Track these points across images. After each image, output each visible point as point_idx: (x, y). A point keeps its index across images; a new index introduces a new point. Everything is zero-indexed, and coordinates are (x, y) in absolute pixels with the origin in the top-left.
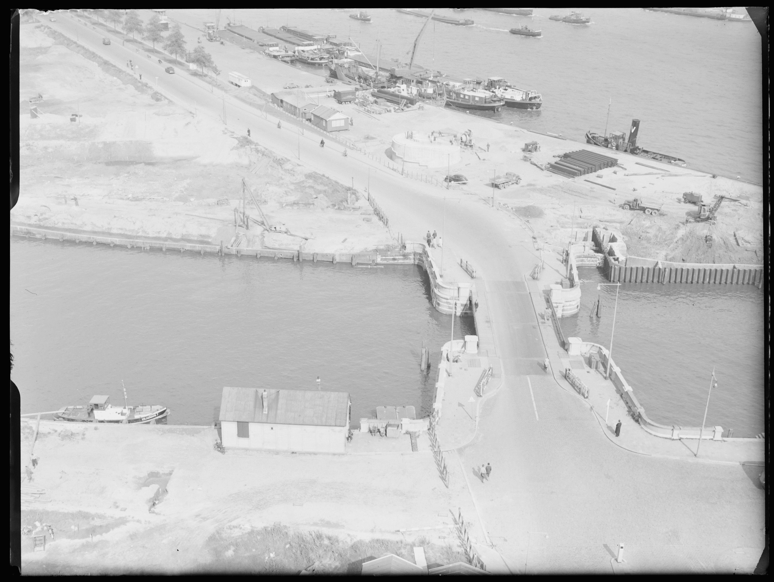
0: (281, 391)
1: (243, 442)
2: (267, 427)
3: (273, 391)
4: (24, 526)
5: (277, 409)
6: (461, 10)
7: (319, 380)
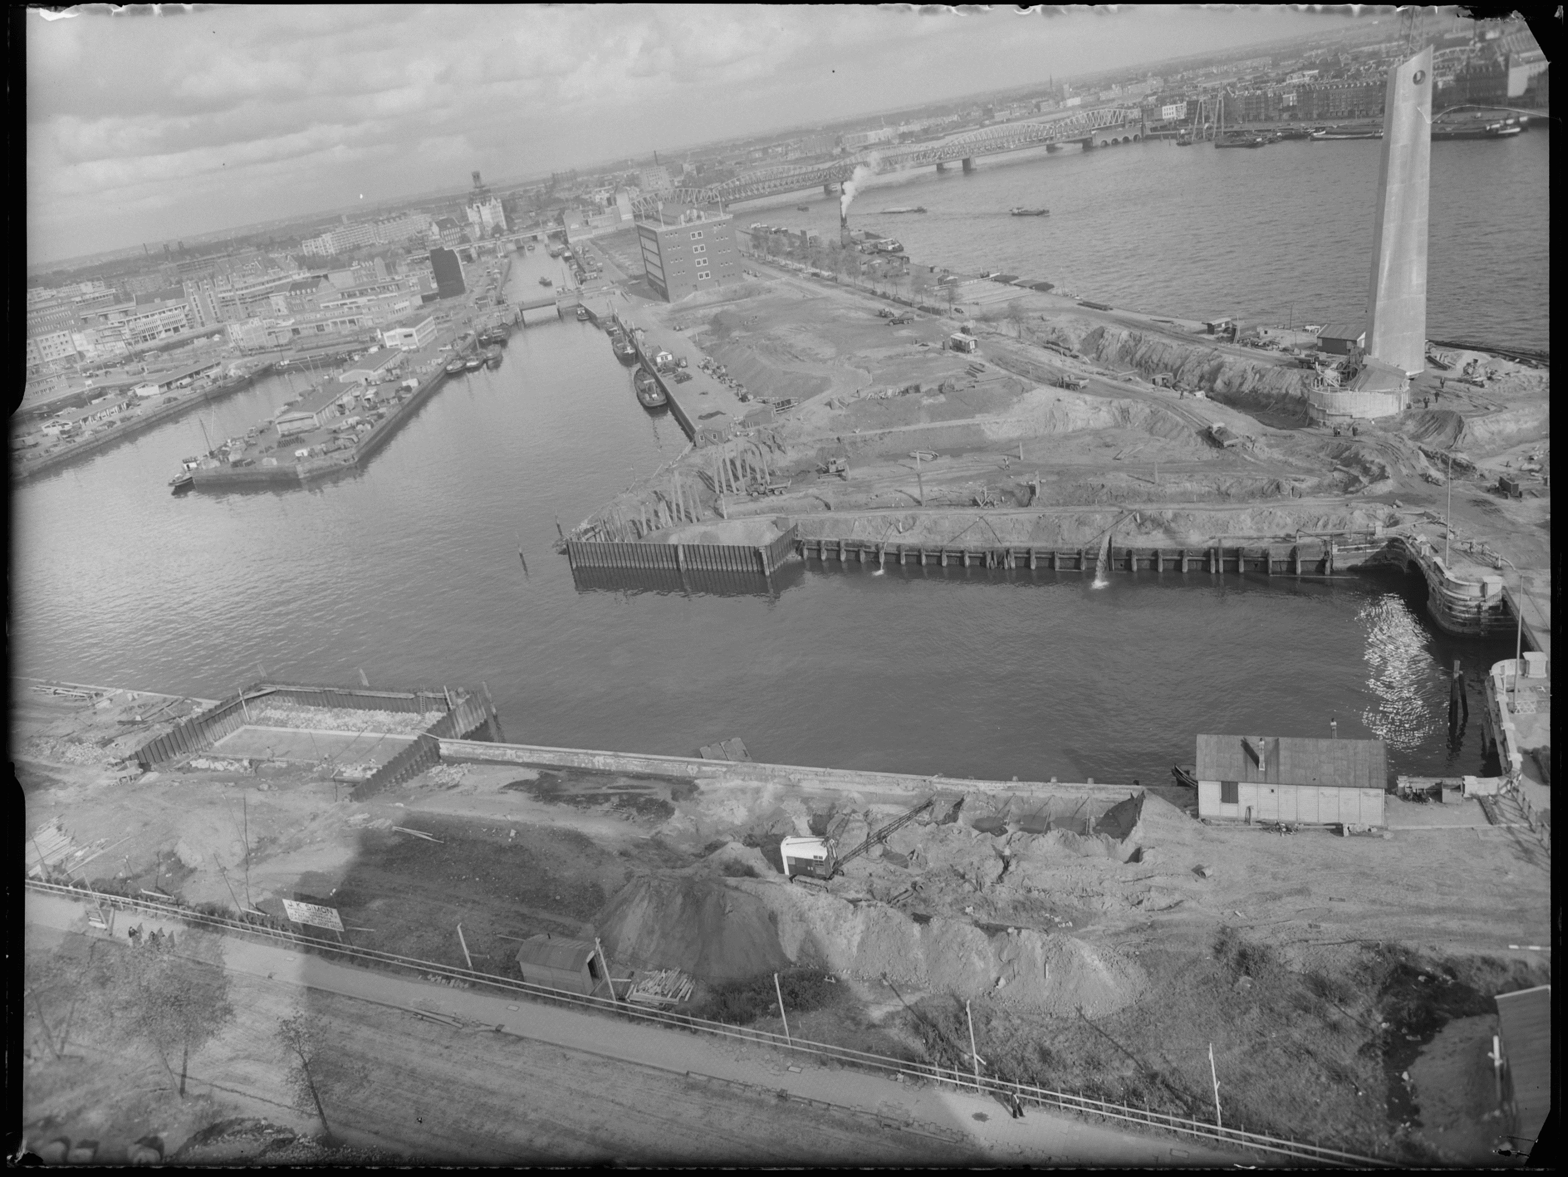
0: (1281, 739)
1: (1230, 810)
2: (1265, 789)
3: (1270, 739)
4: (1541, 929)
5: (1278, 765)
6: (1119, 10)
7: (1334, 723)
